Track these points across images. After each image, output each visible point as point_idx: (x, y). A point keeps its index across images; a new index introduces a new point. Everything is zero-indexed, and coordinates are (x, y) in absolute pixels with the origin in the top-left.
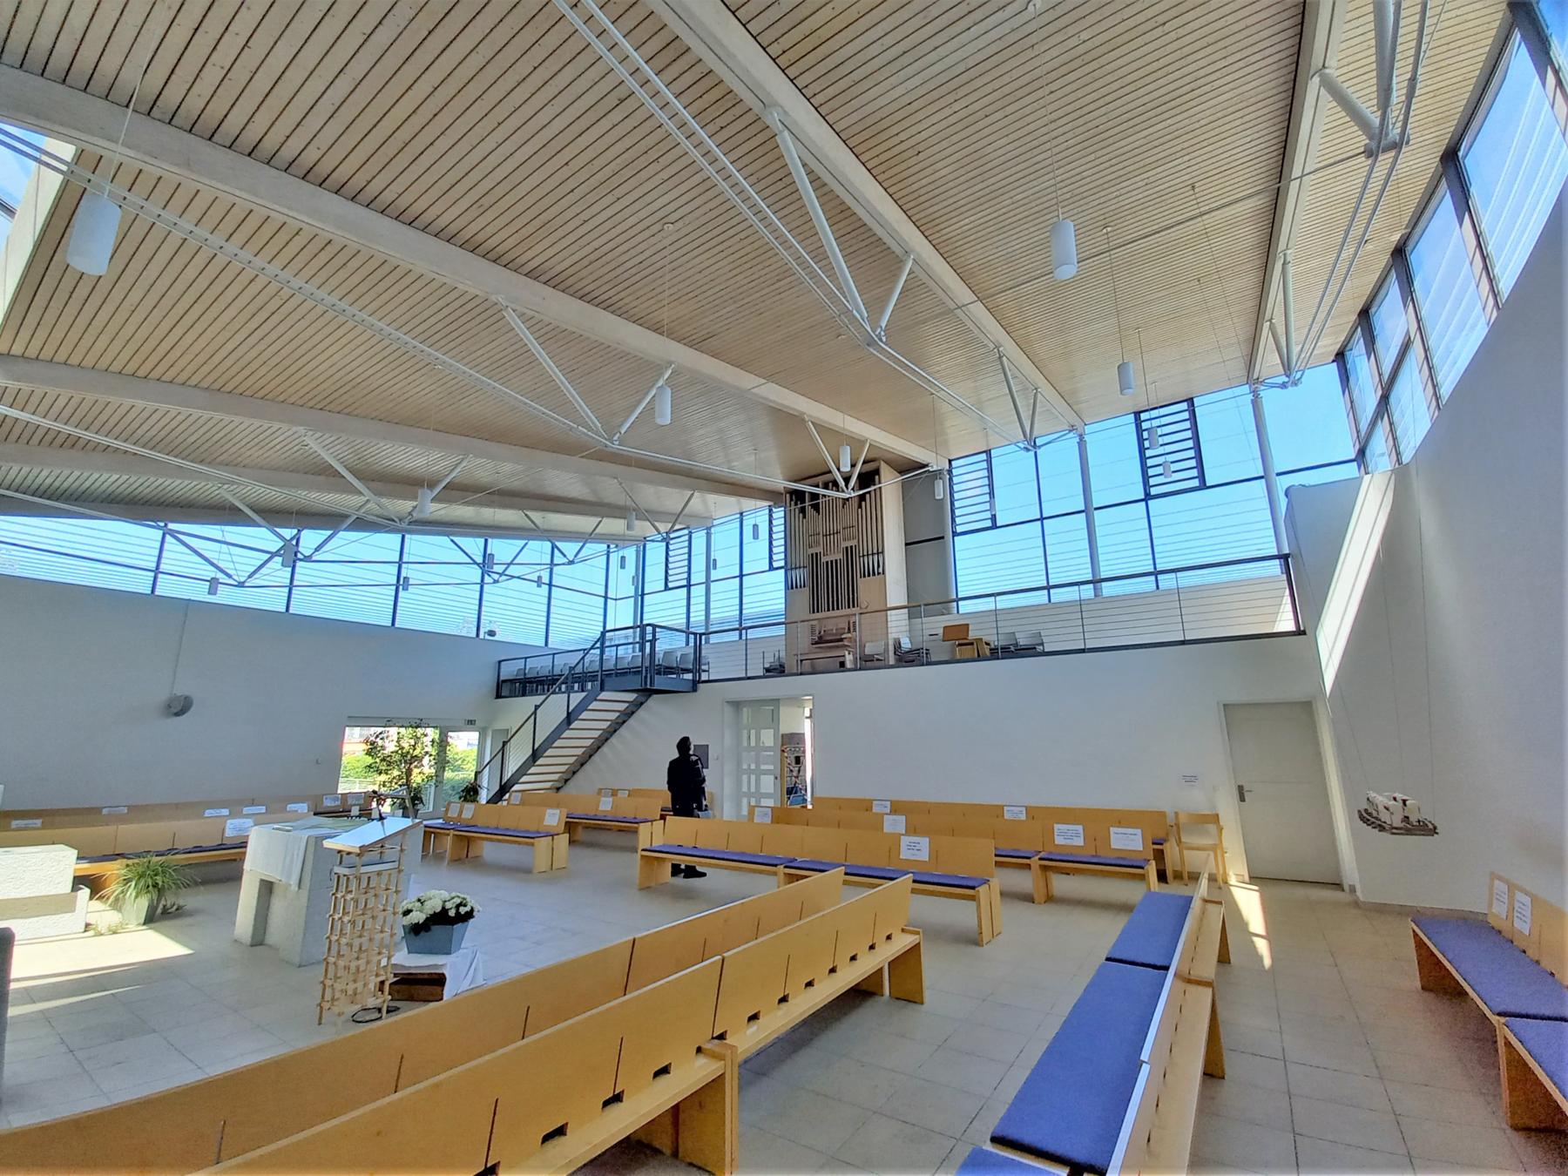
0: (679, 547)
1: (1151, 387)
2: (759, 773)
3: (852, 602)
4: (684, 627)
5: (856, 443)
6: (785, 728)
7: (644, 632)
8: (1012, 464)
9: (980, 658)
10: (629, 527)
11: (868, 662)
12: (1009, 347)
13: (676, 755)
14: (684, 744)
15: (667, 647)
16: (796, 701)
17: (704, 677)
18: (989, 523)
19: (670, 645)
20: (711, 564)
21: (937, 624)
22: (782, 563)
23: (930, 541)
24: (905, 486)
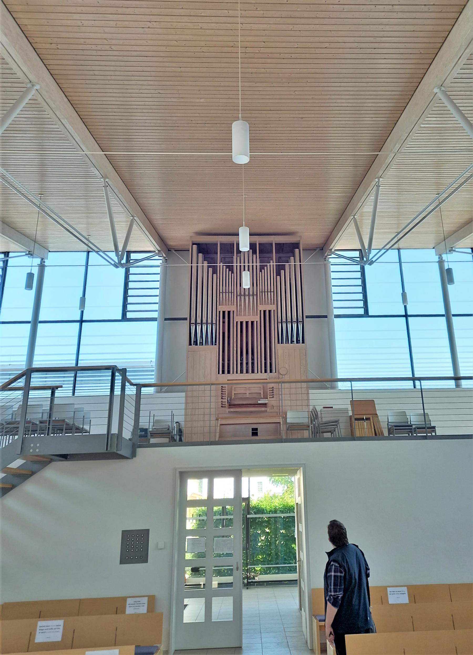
3: (269, 367)
18: (362, 312)
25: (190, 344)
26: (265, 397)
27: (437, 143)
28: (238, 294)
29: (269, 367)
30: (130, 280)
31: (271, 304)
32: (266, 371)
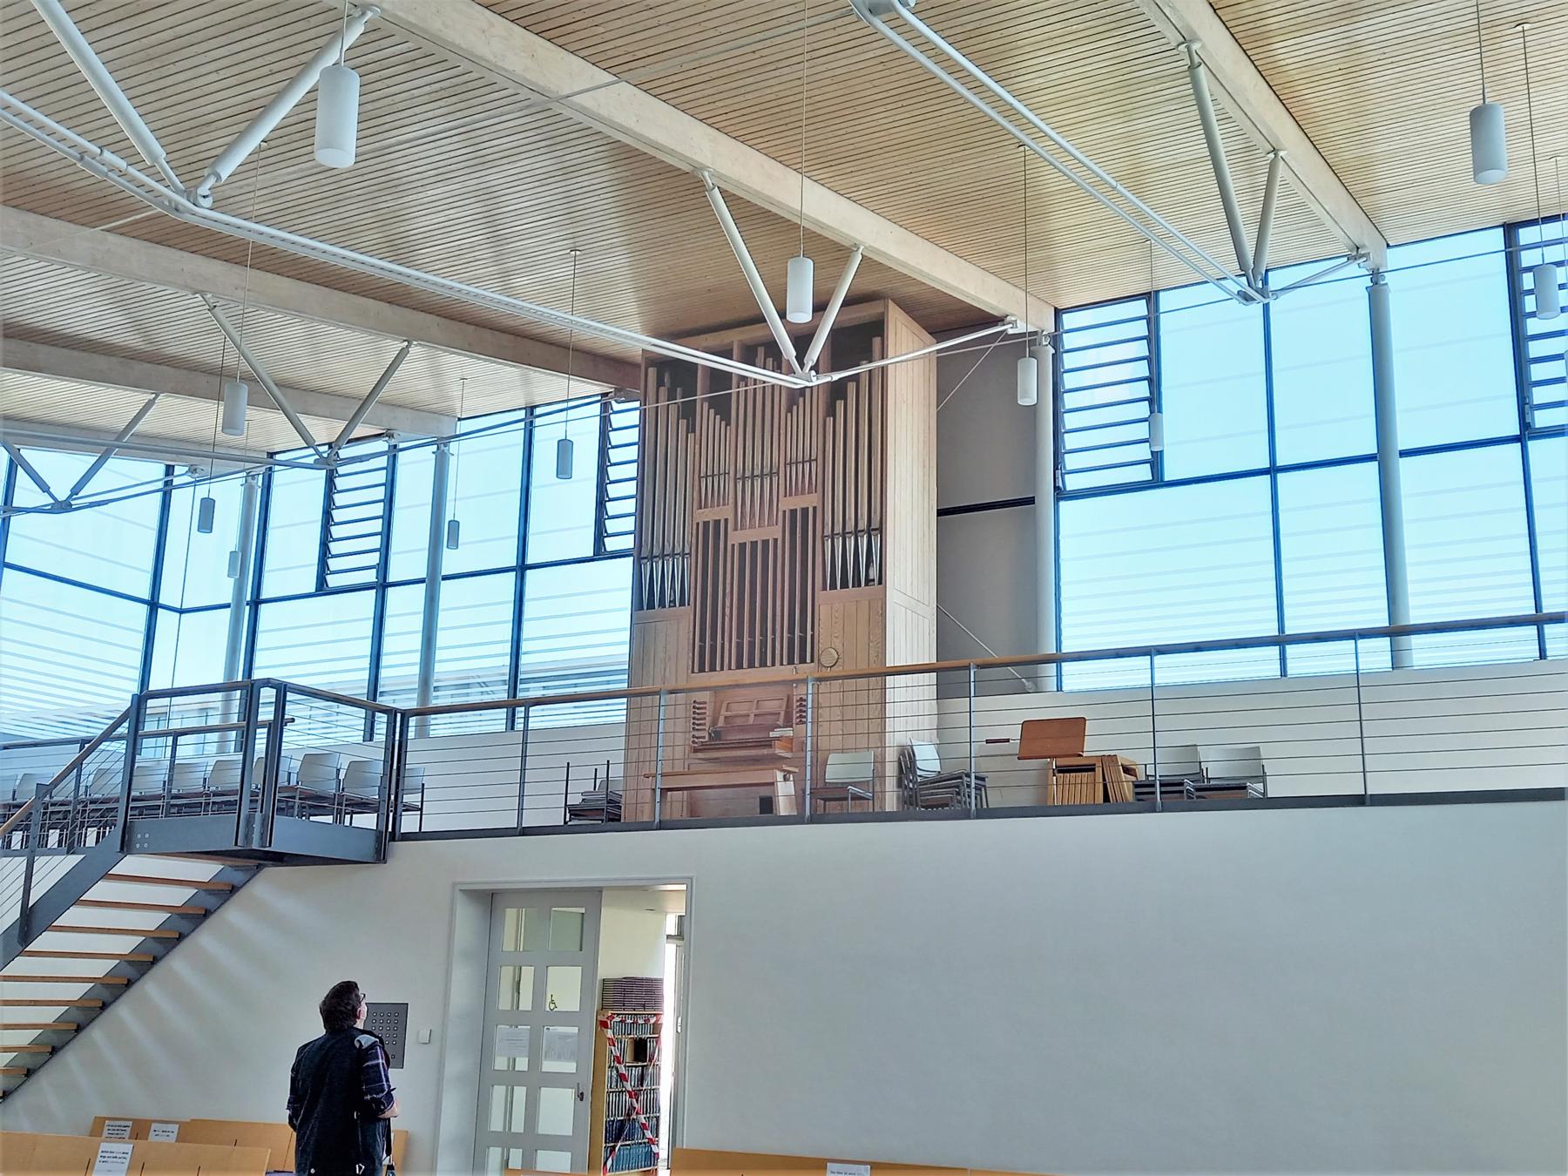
0: (359, 487)
1: (1545, 167)
2: (536, 1081)
3: (800, 651)
4: (361, 692)
5: (830, 252)
6: (612, 966)
7: (255, 702)
8: (1207, 332)
9: (1108, 804)
10: (230, 424)
11: (831, 803)
12: (1215, 42)
13: (316, 1029)
14: (340, 1003)
15: (314, 743)
16: (643, 893)
17: (409, 823)
18: (1144, 473)
19: (321, 737)
20: (442, 533)
21: (1002, 716)
22: (628, 542)
23: (998, 504)
24: (946, 368)
26: (788, 723)
27: (169, 92)
29: (800, 651)
30: (1069, 467)
32: (791, 662)
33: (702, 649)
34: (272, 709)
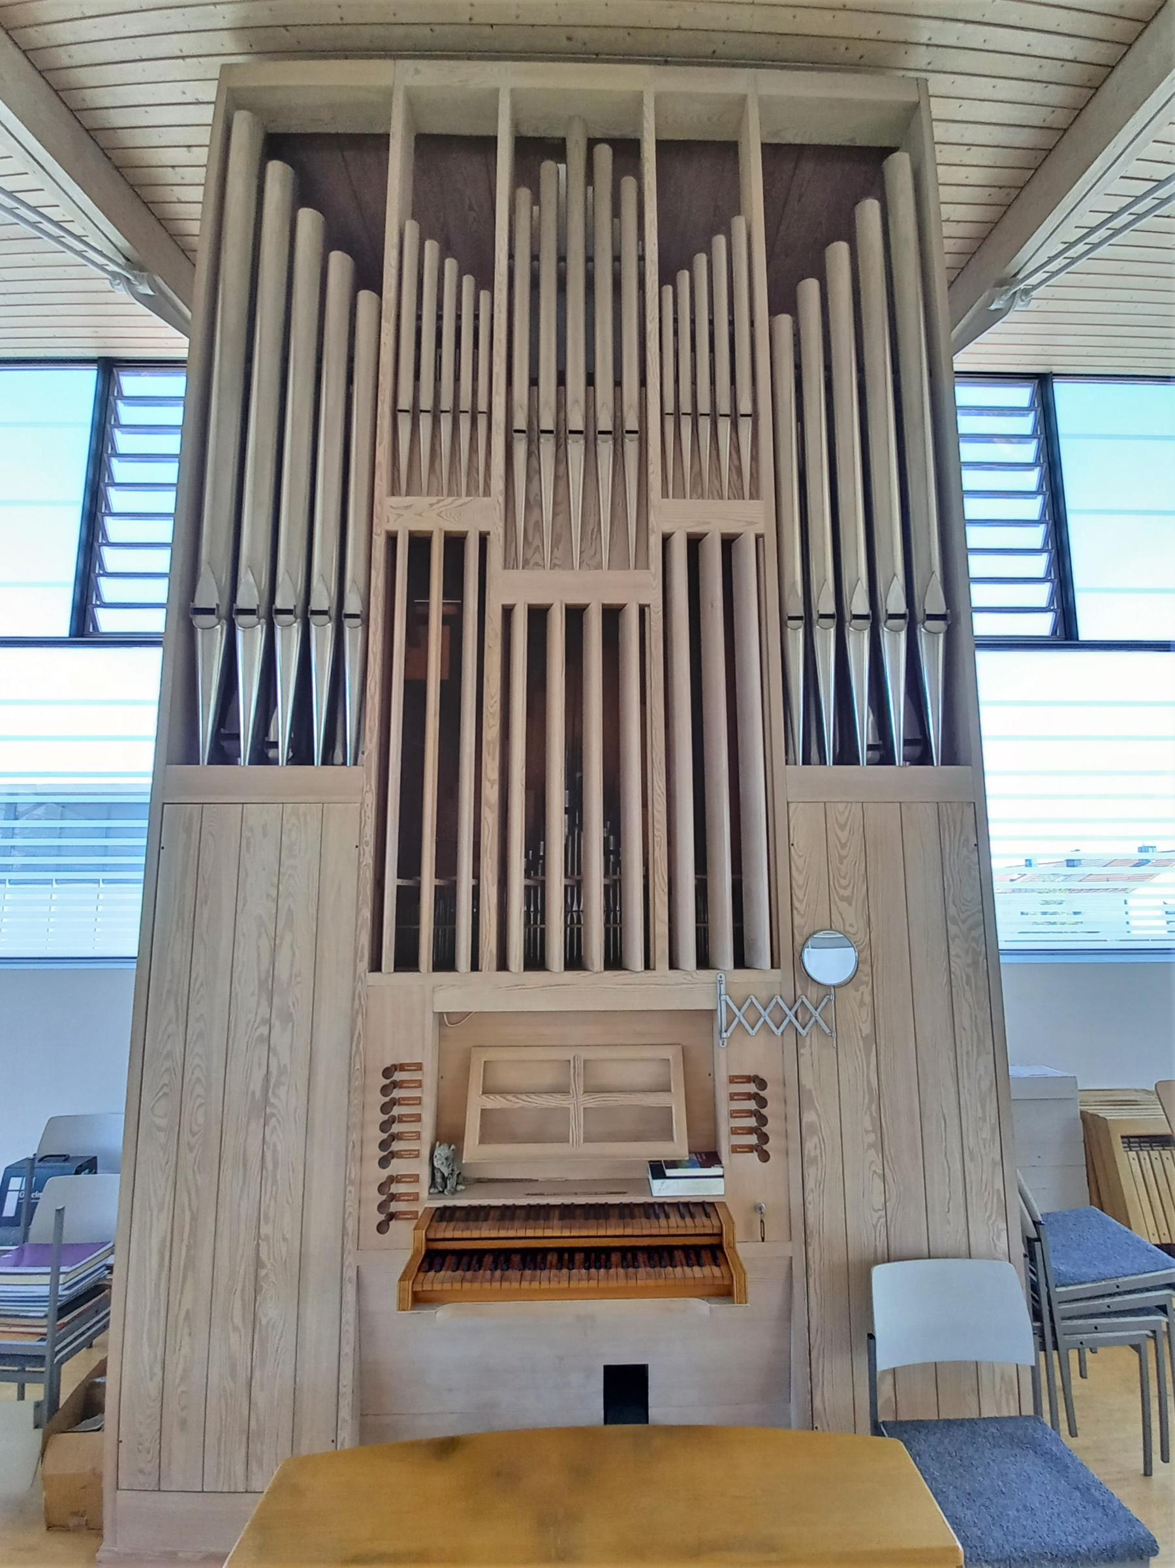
3: (728, 934)
18: (1043, 625)
25: (191, 757)
28: (520, 422)
29: (728, 934)
31: (738, 494)
33: (408, 899)
34: (141, 886)
